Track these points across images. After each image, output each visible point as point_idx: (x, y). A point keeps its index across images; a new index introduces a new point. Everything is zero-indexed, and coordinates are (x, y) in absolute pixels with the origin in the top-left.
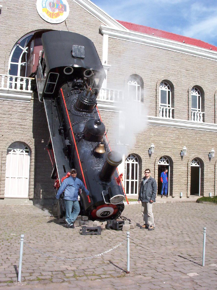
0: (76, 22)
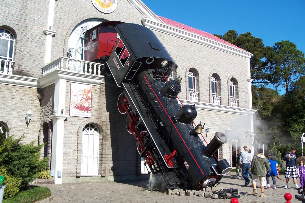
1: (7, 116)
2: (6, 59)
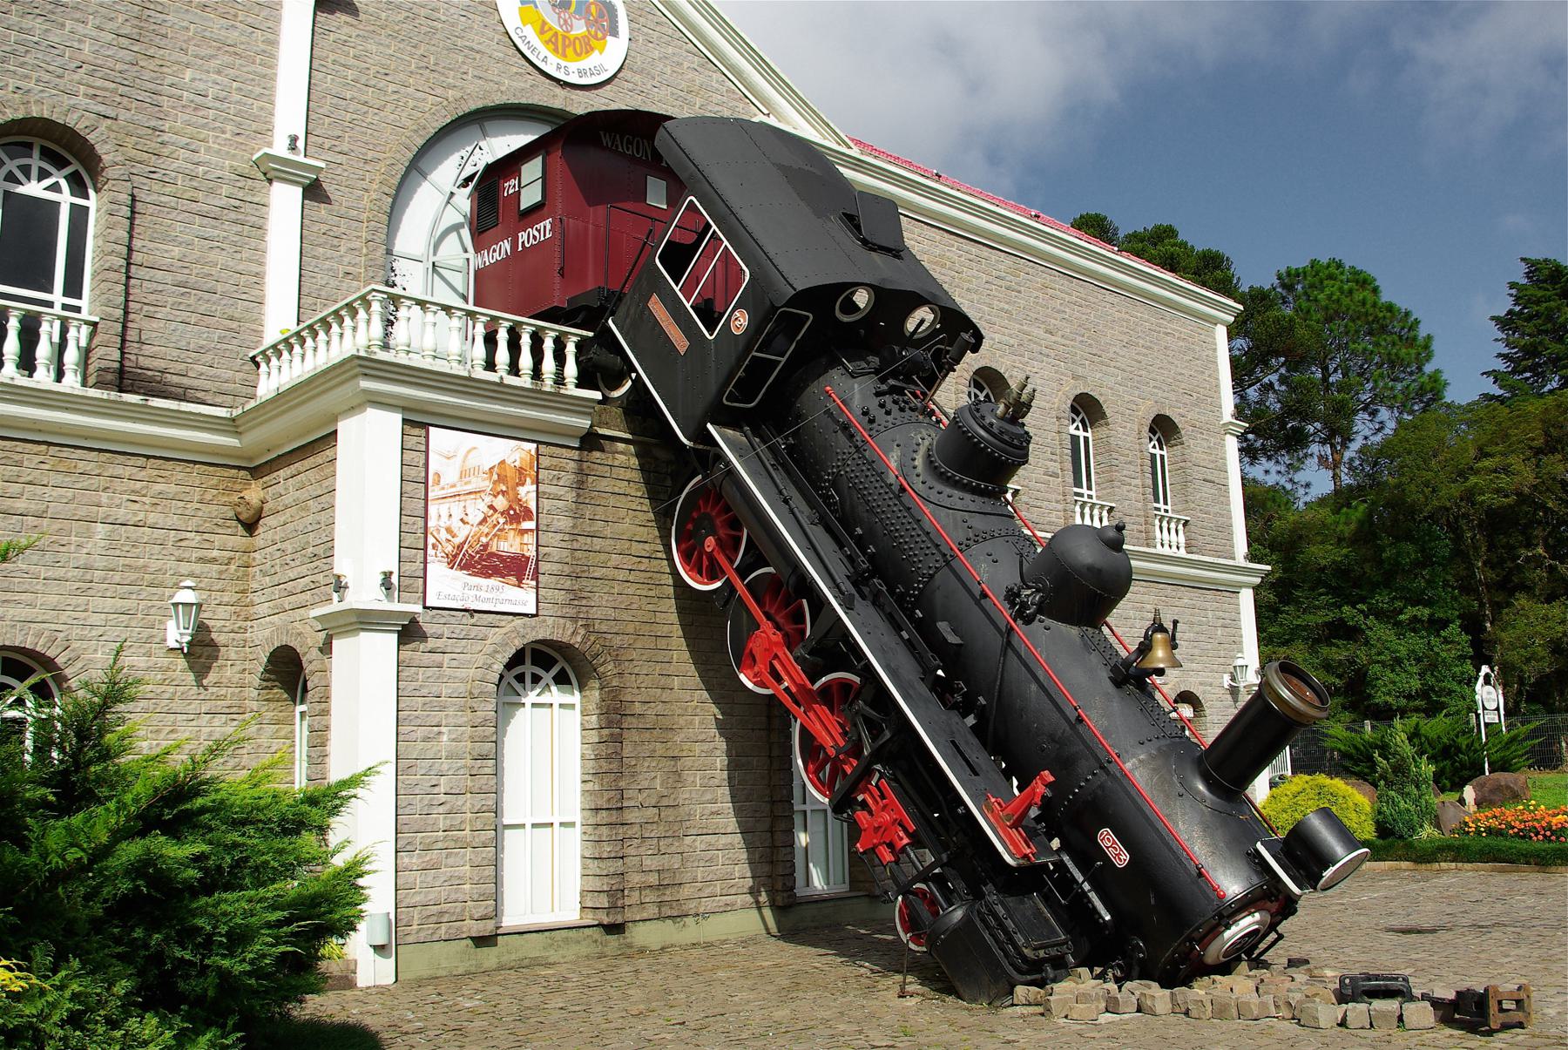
0: (656, 90)
1: (63, 618)
2: (50, 304)
